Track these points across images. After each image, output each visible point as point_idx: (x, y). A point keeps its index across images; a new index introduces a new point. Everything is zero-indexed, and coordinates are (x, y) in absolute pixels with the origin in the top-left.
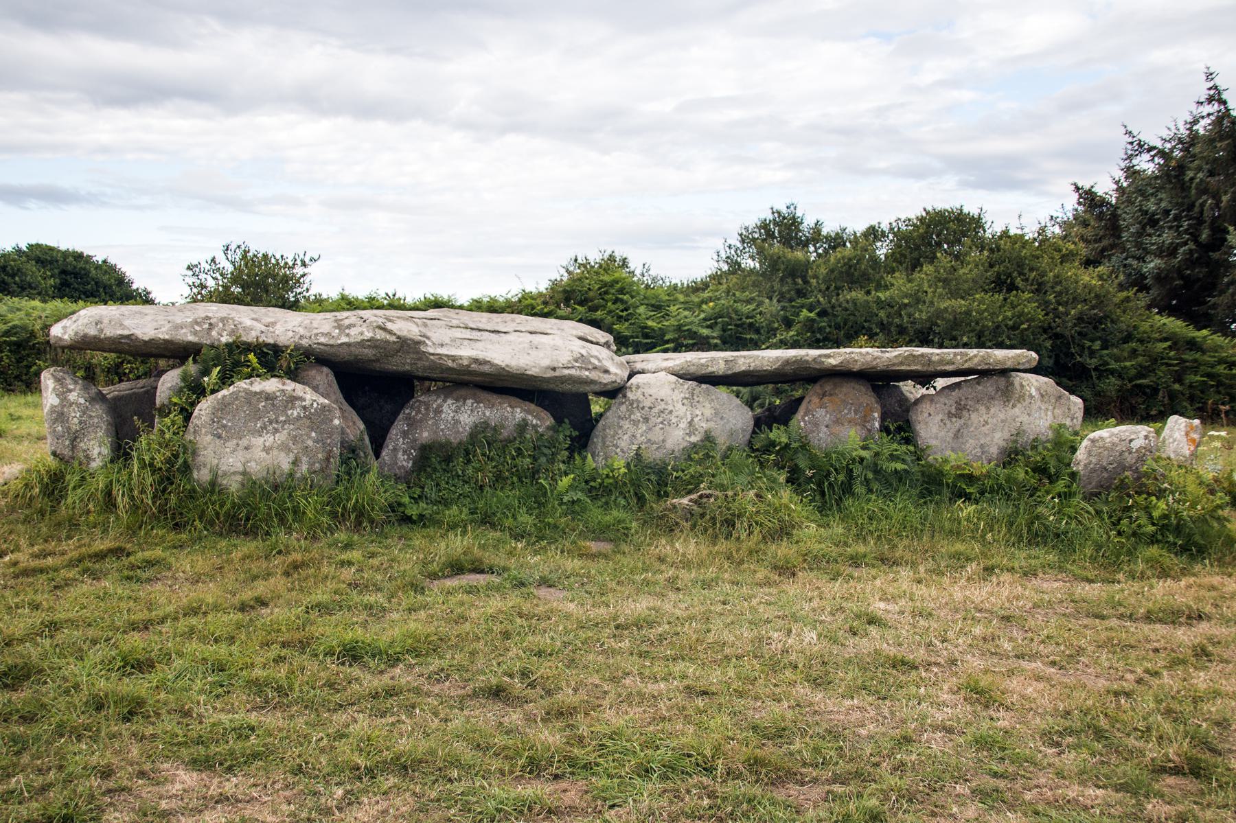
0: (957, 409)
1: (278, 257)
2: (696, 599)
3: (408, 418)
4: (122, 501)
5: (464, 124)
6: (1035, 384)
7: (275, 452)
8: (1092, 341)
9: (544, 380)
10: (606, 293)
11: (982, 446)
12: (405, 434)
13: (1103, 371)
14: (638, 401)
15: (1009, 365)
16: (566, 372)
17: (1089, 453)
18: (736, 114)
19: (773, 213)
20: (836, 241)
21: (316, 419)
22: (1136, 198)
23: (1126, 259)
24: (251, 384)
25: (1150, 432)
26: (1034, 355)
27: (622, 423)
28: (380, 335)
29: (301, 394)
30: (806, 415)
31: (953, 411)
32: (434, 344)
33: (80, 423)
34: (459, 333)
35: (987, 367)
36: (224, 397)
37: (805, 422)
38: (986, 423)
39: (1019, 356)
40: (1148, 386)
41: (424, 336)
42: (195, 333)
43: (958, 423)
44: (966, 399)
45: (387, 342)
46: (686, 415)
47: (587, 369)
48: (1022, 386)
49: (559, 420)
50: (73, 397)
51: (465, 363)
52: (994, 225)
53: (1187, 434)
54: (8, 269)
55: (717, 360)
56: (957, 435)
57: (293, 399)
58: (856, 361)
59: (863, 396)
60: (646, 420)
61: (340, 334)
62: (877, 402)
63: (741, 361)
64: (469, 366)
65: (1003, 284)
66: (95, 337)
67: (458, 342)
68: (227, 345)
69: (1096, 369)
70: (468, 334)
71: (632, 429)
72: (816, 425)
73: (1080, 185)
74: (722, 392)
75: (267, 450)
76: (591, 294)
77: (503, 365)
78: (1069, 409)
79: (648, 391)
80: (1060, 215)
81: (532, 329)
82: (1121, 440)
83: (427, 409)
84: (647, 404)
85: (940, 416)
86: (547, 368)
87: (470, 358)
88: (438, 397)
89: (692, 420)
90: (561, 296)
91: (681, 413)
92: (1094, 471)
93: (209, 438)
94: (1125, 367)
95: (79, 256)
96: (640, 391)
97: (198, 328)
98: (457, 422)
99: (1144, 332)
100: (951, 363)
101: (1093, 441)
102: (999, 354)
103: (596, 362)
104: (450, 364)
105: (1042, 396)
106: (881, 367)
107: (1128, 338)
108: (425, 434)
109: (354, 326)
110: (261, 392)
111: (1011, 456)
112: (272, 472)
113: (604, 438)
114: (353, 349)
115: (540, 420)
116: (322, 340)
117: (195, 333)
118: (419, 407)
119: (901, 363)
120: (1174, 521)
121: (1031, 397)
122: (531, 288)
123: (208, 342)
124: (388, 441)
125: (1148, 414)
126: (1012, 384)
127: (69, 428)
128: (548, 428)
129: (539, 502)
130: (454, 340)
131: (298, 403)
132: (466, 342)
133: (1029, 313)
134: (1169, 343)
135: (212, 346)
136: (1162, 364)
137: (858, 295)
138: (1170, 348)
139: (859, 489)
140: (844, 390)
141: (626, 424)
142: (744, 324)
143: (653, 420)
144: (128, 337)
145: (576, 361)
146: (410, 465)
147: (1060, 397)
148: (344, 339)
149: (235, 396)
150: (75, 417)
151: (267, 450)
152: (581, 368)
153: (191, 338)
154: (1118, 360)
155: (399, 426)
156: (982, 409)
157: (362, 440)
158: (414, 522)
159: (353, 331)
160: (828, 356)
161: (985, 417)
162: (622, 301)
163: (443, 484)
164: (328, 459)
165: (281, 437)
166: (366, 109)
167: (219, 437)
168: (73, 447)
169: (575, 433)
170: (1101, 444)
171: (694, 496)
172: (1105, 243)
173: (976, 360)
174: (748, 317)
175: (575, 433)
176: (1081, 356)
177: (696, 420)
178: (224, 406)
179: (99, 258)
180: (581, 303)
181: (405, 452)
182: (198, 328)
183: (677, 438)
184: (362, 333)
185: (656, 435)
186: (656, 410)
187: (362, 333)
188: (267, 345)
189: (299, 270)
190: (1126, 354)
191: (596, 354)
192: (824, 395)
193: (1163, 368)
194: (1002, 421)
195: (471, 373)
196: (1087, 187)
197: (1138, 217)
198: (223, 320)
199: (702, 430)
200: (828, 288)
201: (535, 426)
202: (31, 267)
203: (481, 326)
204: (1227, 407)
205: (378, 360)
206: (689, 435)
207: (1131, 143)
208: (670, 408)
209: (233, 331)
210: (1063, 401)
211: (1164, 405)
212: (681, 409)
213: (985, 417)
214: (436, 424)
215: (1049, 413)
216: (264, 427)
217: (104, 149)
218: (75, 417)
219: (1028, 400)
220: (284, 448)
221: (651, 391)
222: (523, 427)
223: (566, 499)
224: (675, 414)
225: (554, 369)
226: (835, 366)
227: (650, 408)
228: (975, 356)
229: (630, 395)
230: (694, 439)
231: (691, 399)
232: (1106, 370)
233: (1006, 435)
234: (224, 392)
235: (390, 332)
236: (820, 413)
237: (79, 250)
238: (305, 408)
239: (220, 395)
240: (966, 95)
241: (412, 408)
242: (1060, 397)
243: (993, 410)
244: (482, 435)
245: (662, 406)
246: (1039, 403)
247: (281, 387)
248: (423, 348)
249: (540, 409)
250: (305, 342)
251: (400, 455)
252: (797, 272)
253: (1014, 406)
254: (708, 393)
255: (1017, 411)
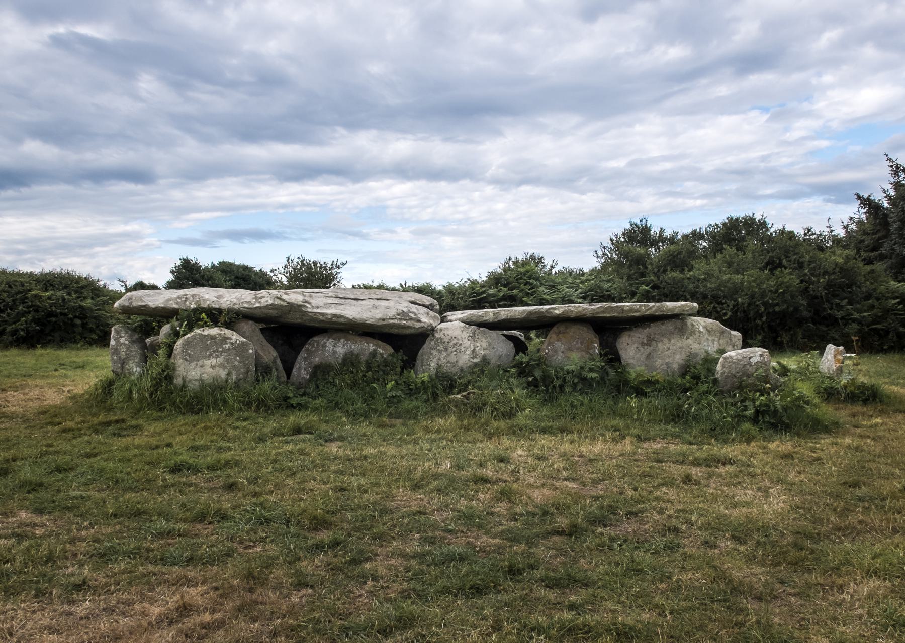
0: (647, 340)
1: (322, 263)
2: (443, 452)
3: (308, 350)
4: (135, 396)
5: (496, 181)
6: (703, 323)
7: (217, 369)
8: (842, 300)
9: (377, 326)
10: (521, 278)
11: (667, 364)
12: (305, 359)
13: (847, 320)
14: (441, 338)
15: (676, 311)
16: (391, 321)
17: (723, 366)
18: (668, 165)
19: (631, 225)
20: (672, 240)
21: (240, 349)
22: (899, 203)
23: (895, 244)
24: (203, 330)
25: (765, 352)
26: (695, 305)
27: (432, 351)
28: (277, 302)
29: (230, 336)
30: (548, 345)
31: (645, 341)
32: (312, 307)
33: (126, 354)
34: (330, 301)
35: (661, 313)
36: (188, 338)
37: (548, 350)
38: (669, 349)
39: (684, 306)
40: (882, 329)
41: (306, 302)
42: (177, 303)
43: (648, 349)
44: (654, 334)
45: (282, 306)
46: (470, 346)
47: (405, 320)
48: (693, 325)
49: (396, 350)
50: (122, 340)
51: (330, 317)
52: (775, 226)
53: (835, 356)
54: (205, 277)
55: (488, 314)
56: (649, 356)
57: (225, 339)
58: (572, 311)
59: (587, 334)
60: (446, 349)
61: (255, 302)
62: (596, 337)
63: (503, 313)
64: (331, 319)
65: (773, 265)
66: (128, 307)
67: (328, 305)
68: (194, 309)
69: (842, 318)
70: (336, 301)
71: (438, 355)
72: (556, 351)
73: (861, 195)
74: (494, 334)
75: (213, 367)
76: (511, 280)
77: (351, 318)
78: (731, 340)
79: (447, 332)
80: (857, 216)
81: (379, 297)
82: (743, 358)
83: (318, 344)
84: (447, 340)
85: (636, 345)
86: (380, 319)
87: (332, 314)
88: (324, 338)
89: (474, 349)
90: (493, 282)
91: (467, 345)
92: (727, 377)
93: (181, 361)
94: (864, 316)
95: (246, 268)
96: (442, 332)
97: (179, 301)
98: (335, 352)
99: (881, 293)
100: (637, 311)
101: (725, 358)
102: (670, 305)
103: (413, 316)
104: (321, 318)
105: (709, 331)
106: (588, 315)
107: (868, 297)
108: (317, 359)
109: (264, 297)
110: (208, 335)
111: (686, 369)
112: (215, 379)
113: (422, 360)
114: (263, 310)
115: (384, 350)
116: (245, 305)
117: (177, 303)
118: (313, 343)
119: (603, 312)
120: (772, 408)
121: (700, 332)
122: (475, 277)
123: (184, 308)
124: (296, 363)
125: (882, 348)
126: (686, 324)
127: (120, 357)
128: (390, 355)
129: (370, 397)
130: (326, 304)
131: (228, 341)
132: (333, 306)
133: (788, 282)
134: (898, 300)
135: (186, 310)
136: (892, 314)
137: (676, 274)
138: (899, 303)
139: (568, 389)
140: (573, 330)
141: (435, 352)
142: (605, 295)
143: (450, 350)
144: (145, 306)
145: (398, 315)
146: (308, 377)
147: (723, 332)
148: (257, 305)
149: (194, 337)
150: (123, 351)
151: (213, 367)
152: (401, 319)
153: (175, 306)
154: (859, 311)
155: (303, 354)
156: (666, 340)
157: (274, 362)
158: (294, 408)
159: (263, 301)
160: (555, 309)
161: (668, 345)
162: (531, 284)
163: (321, 387)
164: (247, 372)
165: (220, 360)
166: (435, 174)
167: (186, 360)
168: (122, 367)
169: (405, 358)
170: (730, 360)
171: (464, 394)
172: (879, 234)
173: (654, 309)
174: (607, 291)
175: (405, 358)
176: (830, 310)
177: (477, 349)
178: (188, 343)
179: (257, 269)
180: (505, 286)
181: (305, 370)
182: (179, 301)
183: (465, 359)
184: (267, 301)
185: (453, 358)
186: (452, 343)
187: (267, 301)
188: (215, 309)
189: (334, 271)
190: (866, 308)
191: (415, 311)
192: (559, 333)
193: (893, 317)
194: (680, 348)
195: (335, 323)
196: (866, 196)
197: (901, 216)
198: (193, 296)
199: (481, 355)
200: (659, 271)
201: (381, 354)
202: (218, 275)
203: (348, 296)
204: (857, 338)
205: (280, 317)
206: (473, 358)
207: (892, 166)
208: (460, 342)
209: (197, 301)
210: (725, 335)
211: (894, 342)
212: (467, 343)
213: (668, 345)
214: (323, 353)
215: (716, 342)
216: (211, 355)
217: (283, 206)
218: (123, 351)
219: (697, 334)
220: (222, 366)
221: (449, 332)
222: (374, 354)
223: (389, 395)
224: (463, 345)
225: (384, 320)
226: (559, 315)
227: (448, 342)
228: (653, 306)
229: (437, 335)
230: (475, 360)
231: (473, 337)
232: (850, 319)
233: (684, 356)
234: (189, 335)
235: (284, 301)
236: (558, 344)
237: (246, 264)
238: (232, 343)
239: (186, 337)
240: (824, 143)
241: (310, 344)
242: (723, 332)
243: (673, 341)
244: (350, 361)
245: (455, 341)
246: (706, 336)
247: (219, 332)
248: (303, 309)
249: (385, 344)
250: (236, 307)
251: (302, 371)
252: (640, 261)
253: (687, 338)
254: (484, 333)
255: (690, 341)
